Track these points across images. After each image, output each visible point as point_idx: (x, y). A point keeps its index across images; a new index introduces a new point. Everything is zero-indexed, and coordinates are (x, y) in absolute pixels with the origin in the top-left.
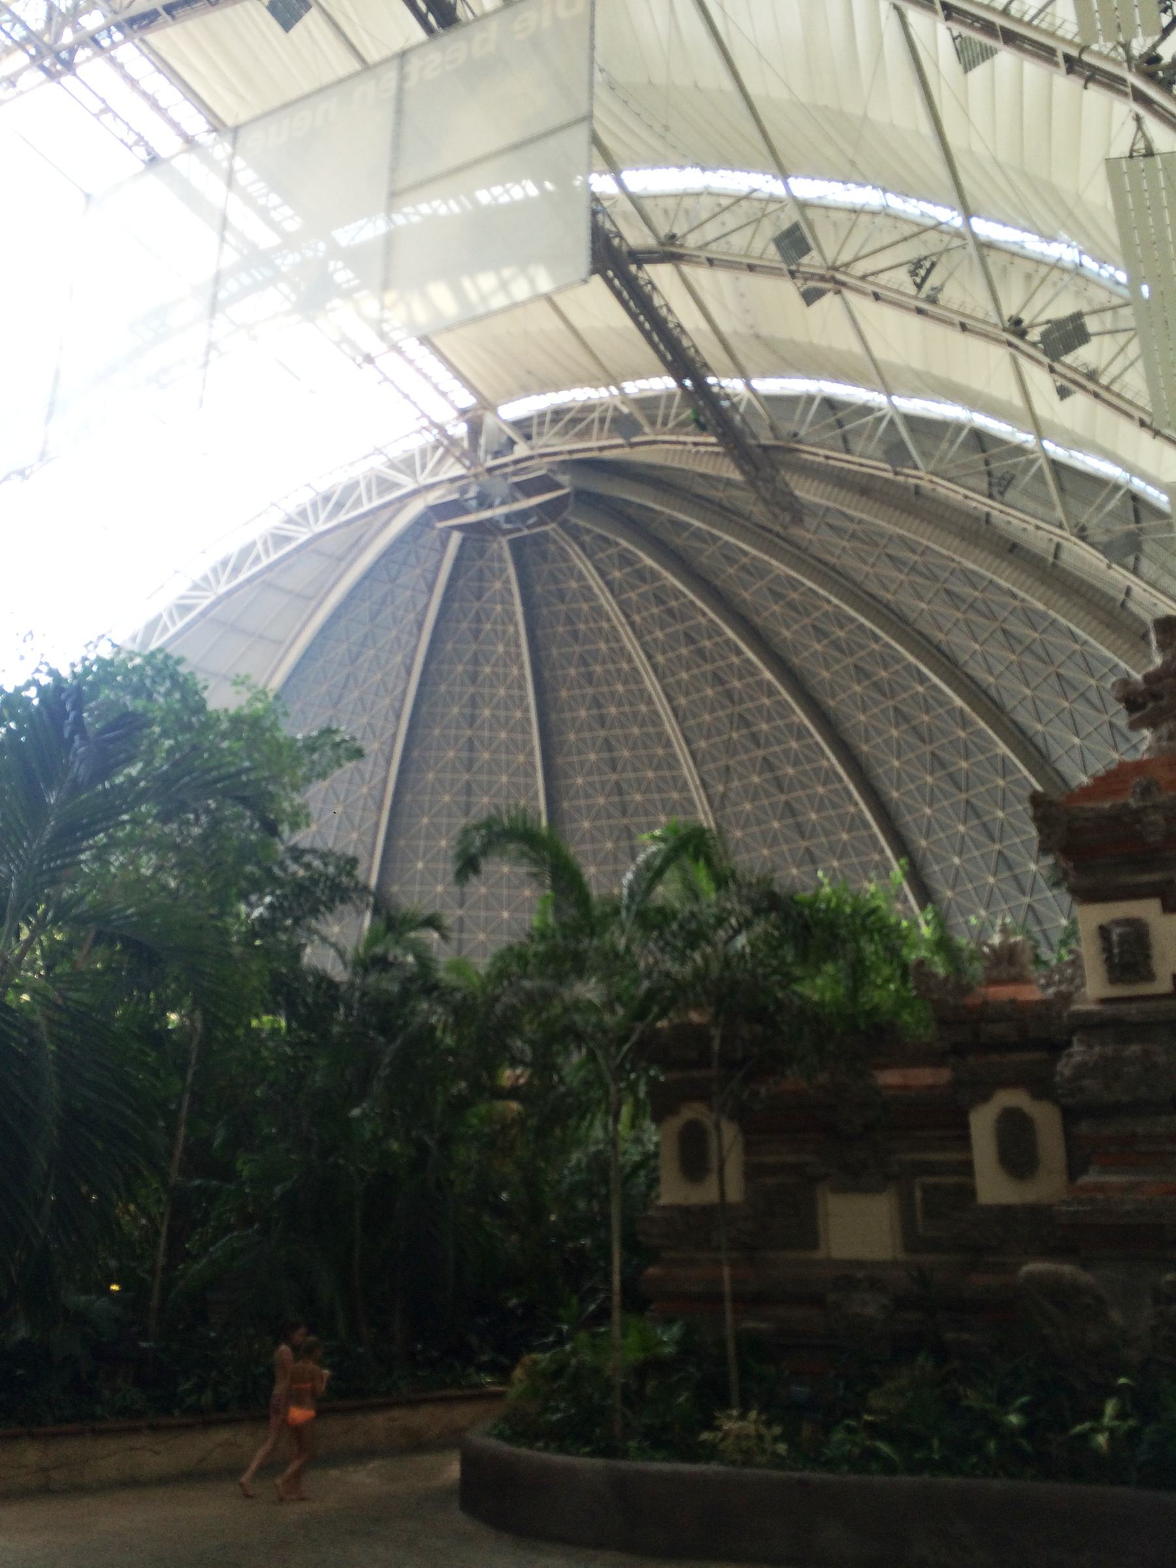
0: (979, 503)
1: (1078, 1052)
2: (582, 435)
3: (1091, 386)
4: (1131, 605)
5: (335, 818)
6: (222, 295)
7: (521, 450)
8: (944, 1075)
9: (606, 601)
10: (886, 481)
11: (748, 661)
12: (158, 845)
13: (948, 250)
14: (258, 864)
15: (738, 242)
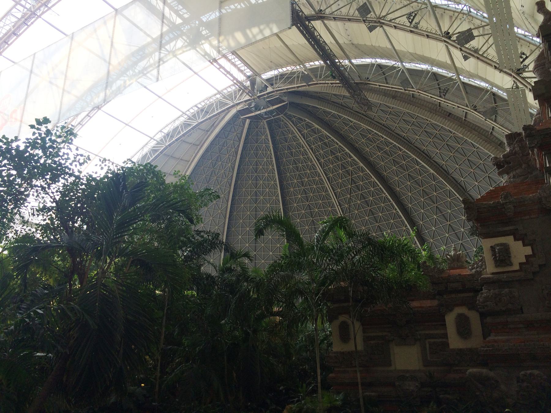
0: (436, 99)
1: (485, 292)
2: (291, 83)
3: (476, 55)
4: (494, 133)
5: (211, 220)
6: (163, 42)
7: (270, 89)
8: (435, 303)
9: (302, 141)
10: (402, 93)
11: (354, 160)
12: (151, 231)
13: (420, 9)
14: (185, 237)
15: (344, 11)
